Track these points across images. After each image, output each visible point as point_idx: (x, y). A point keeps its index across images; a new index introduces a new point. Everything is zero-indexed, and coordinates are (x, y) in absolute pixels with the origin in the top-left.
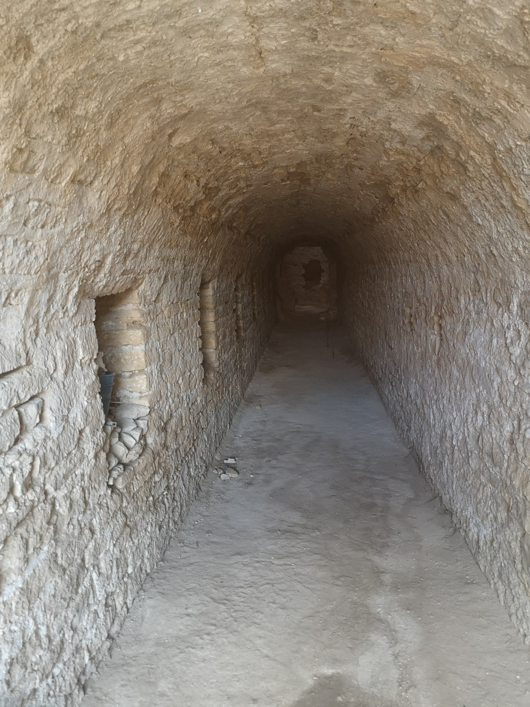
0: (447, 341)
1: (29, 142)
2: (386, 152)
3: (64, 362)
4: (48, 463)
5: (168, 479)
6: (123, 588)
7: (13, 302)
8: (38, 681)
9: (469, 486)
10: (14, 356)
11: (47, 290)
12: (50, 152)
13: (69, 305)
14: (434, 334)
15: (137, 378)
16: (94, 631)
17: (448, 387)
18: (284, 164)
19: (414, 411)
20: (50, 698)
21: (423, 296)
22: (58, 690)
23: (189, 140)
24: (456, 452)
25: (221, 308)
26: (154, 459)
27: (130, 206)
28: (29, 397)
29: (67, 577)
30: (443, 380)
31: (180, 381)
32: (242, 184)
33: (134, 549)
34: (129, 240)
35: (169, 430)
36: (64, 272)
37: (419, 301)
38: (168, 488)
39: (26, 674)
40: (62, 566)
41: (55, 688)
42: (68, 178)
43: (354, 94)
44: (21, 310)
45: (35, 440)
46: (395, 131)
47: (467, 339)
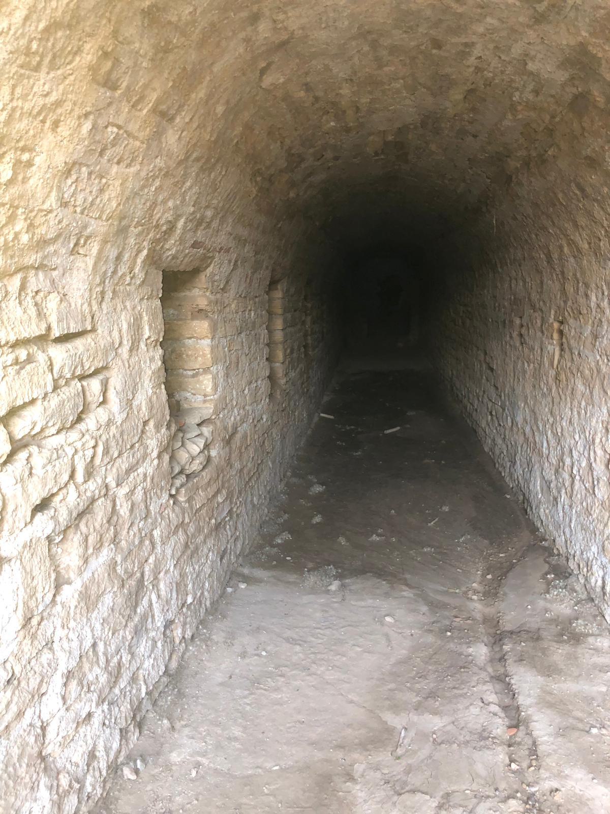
0: (570, 349)
1: (116, 45)
2: (513, 108)
3: (129, 337)
4: (111, 452)
5: (231, 503)
6: (182, 619)
7: (81, 251)
8: (94, 705)
9: (593, 521)
10: (80, 317)
11: (116, 244)
12: (135, 64)
13: (137, 270)
14: (552, 344)
15: (201, 378)
16: (152, 661)
17: (569, 404)
18: (382, 128)
19: (521, 440)
20: (105, 728)
21: (539, 300)
22: (113, 720)
23: (281, 80)
24: (577, 483)
25: (290, 316)
26: (218, 476)
27: (208, 160)
28: (93, 369)
29: (126, 591)
30: (563, 397)
31: (246, 392)
32: (329, 155)
33: (194, 576)
34: (204, 204)
35: (234, 447)
36: (135, 228)
37: (533, 307)
38: (230, 512)
39: (83, 693)
40: (120, 576)
41: (111, 718)
42: (150, 105)
43: (489, 20)
44: (88, 263)
45: (98, 422)
46: (532, 73)
47: (598, 343)
